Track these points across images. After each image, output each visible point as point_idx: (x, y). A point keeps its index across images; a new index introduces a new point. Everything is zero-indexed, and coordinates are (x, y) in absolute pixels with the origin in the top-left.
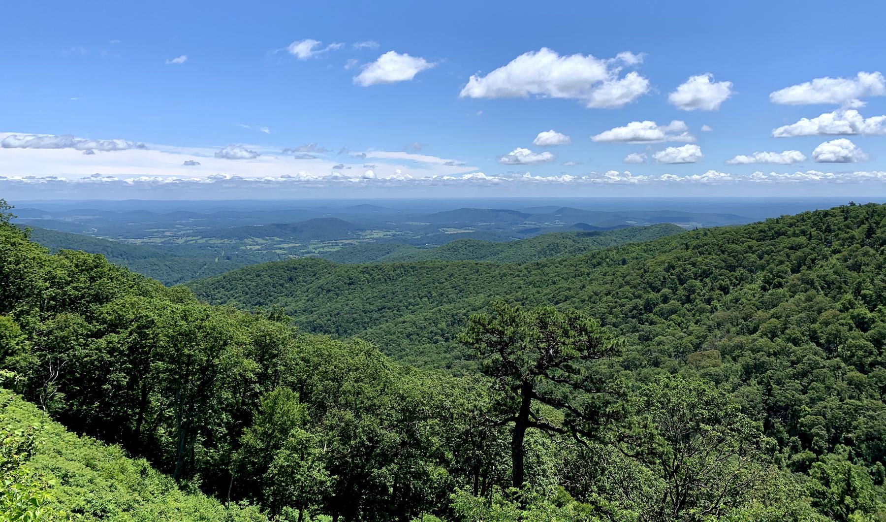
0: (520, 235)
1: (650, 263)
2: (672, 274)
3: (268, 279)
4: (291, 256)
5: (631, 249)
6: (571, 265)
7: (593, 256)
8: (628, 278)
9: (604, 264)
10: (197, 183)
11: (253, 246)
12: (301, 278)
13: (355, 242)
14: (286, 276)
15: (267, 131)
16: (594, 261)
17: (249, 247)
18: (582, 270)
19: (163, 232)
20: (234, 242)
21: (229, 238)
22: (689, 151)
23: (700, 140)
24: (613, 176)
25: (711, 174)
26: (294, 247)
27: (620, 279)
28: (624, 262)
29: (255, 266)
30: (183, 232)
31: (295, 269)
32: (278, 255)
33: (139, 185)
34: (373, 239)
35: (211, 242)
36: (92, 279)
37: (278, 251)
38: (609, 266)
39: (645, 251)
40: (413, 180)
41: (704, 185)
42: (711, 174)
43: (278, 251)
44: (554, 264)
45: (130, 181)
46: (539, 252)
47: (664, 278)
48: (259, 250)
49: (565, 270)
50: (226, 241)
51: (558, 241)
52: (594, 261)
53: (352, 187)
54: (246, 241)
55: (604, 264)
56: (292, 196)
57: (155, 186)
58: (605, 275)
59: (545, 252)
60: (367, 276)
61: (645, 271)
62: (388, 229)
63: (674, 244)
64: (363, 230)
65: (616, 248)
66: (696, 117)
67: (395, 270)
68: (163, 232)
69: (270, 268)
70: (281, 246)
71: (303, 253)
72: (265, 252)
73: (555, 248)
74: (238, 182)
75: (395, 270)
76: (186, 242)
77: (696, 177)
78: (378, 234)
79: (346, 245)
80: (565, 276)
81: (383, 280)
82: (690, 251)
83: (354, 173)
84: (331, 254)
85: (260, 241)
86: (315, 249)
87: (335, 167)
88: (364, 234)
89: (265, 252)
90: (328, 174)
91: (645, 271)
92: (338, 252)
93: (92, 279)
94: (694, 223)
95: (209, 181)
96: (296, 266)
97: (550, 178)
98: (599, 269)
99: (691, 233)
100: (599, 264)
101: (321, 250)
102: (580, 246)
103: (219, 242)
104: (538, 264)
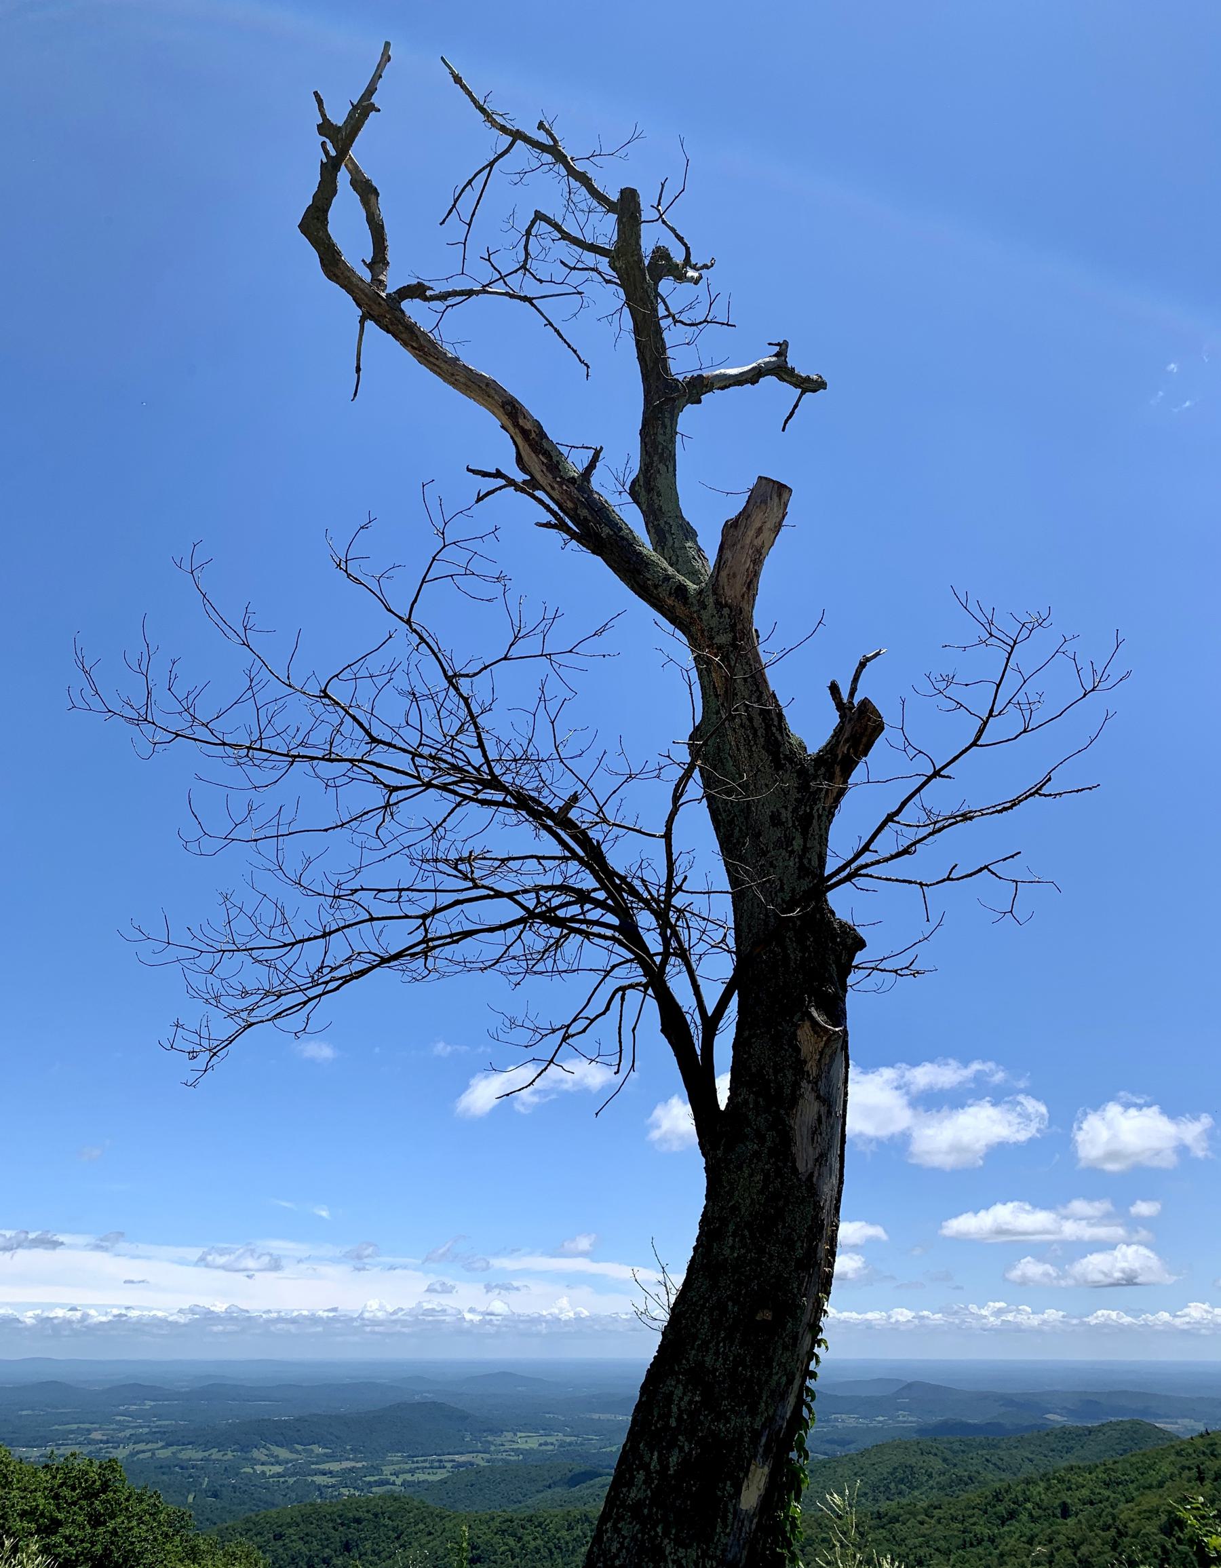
0: (827, 1447)
1: (1125, 1512)
2: (1180, 1541)
3: (299, 1545)
4: (345, 1491)
5: (1075, 1479)
6: (954, 1519)
7: (998, 1497)
8: (1084, 1549)
9: (1024, 1517)
10: (163, 1322)
11: (269, 1464)
12: (368, 1545)
13: (480, 1460)
14: (336, 1537)
15: (324, 1214)
16: (1000, 1508)
17: (259, 1468)
18: (977, 1529)
19: (89, 1431)
20: (230, 1455)
21: (221, 1447)
22: (1132, 1257)
23: (1156, 1234)
24: (989, 1312)
25: (1196, 1311)
26: (352, 1470)
27: (1068, 1553)
28: (1065, 1512)
29: (273, 1512)
30: (128, 1433)
31: (358, 1521)
32: (319, 1488)
33: (48, 1327)
34: (517, 1451)
35: (184, 1455)
36: (96, 1520)
37: (319, 1480)
38: (1033, 1519)
39: (1107, 1485)
40: (594, 1319)
41: (1185, 1333)
42: (1196, 1311)
43: (319, 1480)
44: (914, 1514)
45: (28, 1317)
46: (875, 1488)
47: (1163, 1548)
48: (279, 1475)
49: (940, 1531)
50: (215, 1454)
51: (912, 1461)
52: (1000, 1508)
53: (461, 1331)
54: (256, 1453)
55: (1024, 1517)
56: (351, 1354)
57: (85, 1330)
58: (1030, 1542)
59: (888, 1488)
60: (511, 1542)
61: (1121, 1534)
62: (548, 1428)
63: (1166, 1468)
64: (498, 1431)
65: (1044, 1477)
66: (1120, 1186)
67: (570, 1528)
68: (89, 1431)
69: (306, 1519)
70: (321, 1467)
71: (370, 1484)
72: (291, 1480)
73: (906, 1477)
74: (240, 1321)
75: (570, 1528)
76: (133, 1454)
77: (1165, 1316)
78: (529, 1442)
79: (460, 1465)
80: (943, 1544)
81: (544, 1552)
82: (1208, 1483)
83: (469, 1301)
84: (429, 1486)
85: (283, 1453)
86: (398, 1473)
87: (430, 1290)
88: (498, 1441)
89: (291, 1480)
90: (409, 1304)
91: (1121, 1534)
92: (443, 1482)
93: (96, 1520)
94: (1186, 1421)
95: (182, 1319)
96: (360, 1514)
97: (870, 1316)
98: (1013, 1526)
99: (1199, 1441)
100: (1012, 1515)
101: (408, 1477)
102: (960, 1471)
103: (200, 1455)
104: (879, 1516)
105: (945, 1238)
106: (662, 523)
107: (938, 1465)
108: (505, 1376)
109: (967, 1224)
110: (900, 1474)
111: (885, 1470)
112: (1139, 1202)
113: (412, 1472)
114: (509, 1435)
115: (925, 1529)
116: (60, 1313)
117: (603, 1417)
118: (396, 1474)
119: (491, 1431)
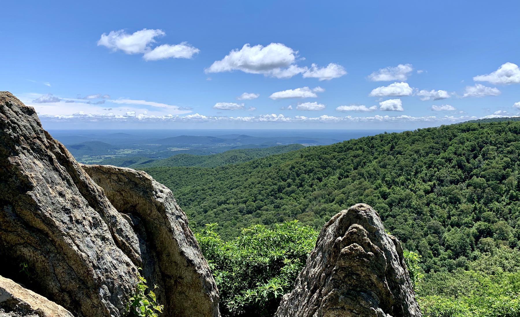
2: (293, 171)
5: (274, 158)
16: (254, 165)
34: (125, 154)
38: (262, 168)
46: (226, 161)
51: (236, 154)
52: (254, 165)
61: (279, 170)
62: (134, 148)
78: (224, 145)
79: (107, 158)
88: (119, 151)
91: (279, 170)
100: (257, 166)
102: (249, 157)
104: (223, 168)
105: (271, 99)
106: (446, 269)
107: (243, 155)
108: (121, 134)
109: (277, 95)
110: (233, 157)
111: (229, 157)
112: (245, 47)
113: (91, 160)
114: (122, 150)
115: (234, 171)
116: (71, 117)
117: (152, 145)
118: (86, 161)
119: (116, 149)
